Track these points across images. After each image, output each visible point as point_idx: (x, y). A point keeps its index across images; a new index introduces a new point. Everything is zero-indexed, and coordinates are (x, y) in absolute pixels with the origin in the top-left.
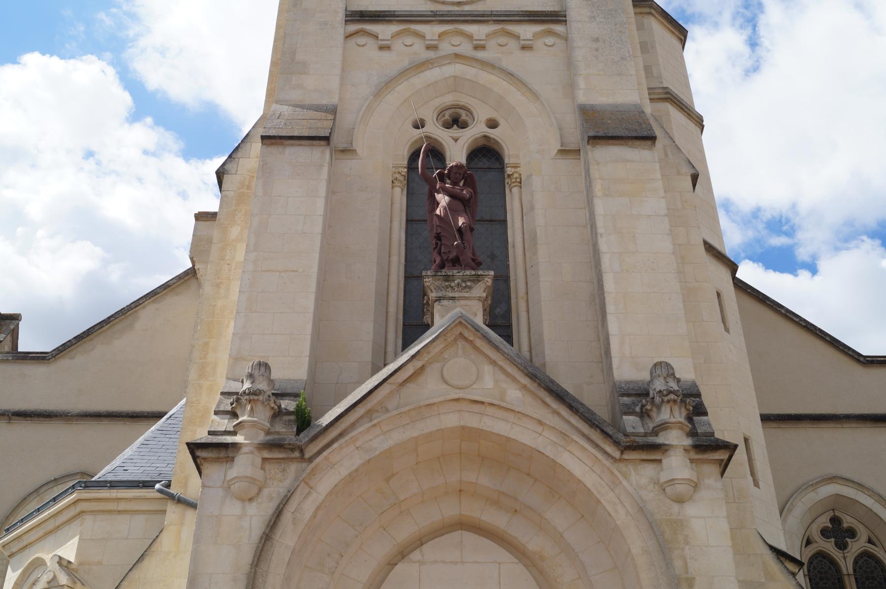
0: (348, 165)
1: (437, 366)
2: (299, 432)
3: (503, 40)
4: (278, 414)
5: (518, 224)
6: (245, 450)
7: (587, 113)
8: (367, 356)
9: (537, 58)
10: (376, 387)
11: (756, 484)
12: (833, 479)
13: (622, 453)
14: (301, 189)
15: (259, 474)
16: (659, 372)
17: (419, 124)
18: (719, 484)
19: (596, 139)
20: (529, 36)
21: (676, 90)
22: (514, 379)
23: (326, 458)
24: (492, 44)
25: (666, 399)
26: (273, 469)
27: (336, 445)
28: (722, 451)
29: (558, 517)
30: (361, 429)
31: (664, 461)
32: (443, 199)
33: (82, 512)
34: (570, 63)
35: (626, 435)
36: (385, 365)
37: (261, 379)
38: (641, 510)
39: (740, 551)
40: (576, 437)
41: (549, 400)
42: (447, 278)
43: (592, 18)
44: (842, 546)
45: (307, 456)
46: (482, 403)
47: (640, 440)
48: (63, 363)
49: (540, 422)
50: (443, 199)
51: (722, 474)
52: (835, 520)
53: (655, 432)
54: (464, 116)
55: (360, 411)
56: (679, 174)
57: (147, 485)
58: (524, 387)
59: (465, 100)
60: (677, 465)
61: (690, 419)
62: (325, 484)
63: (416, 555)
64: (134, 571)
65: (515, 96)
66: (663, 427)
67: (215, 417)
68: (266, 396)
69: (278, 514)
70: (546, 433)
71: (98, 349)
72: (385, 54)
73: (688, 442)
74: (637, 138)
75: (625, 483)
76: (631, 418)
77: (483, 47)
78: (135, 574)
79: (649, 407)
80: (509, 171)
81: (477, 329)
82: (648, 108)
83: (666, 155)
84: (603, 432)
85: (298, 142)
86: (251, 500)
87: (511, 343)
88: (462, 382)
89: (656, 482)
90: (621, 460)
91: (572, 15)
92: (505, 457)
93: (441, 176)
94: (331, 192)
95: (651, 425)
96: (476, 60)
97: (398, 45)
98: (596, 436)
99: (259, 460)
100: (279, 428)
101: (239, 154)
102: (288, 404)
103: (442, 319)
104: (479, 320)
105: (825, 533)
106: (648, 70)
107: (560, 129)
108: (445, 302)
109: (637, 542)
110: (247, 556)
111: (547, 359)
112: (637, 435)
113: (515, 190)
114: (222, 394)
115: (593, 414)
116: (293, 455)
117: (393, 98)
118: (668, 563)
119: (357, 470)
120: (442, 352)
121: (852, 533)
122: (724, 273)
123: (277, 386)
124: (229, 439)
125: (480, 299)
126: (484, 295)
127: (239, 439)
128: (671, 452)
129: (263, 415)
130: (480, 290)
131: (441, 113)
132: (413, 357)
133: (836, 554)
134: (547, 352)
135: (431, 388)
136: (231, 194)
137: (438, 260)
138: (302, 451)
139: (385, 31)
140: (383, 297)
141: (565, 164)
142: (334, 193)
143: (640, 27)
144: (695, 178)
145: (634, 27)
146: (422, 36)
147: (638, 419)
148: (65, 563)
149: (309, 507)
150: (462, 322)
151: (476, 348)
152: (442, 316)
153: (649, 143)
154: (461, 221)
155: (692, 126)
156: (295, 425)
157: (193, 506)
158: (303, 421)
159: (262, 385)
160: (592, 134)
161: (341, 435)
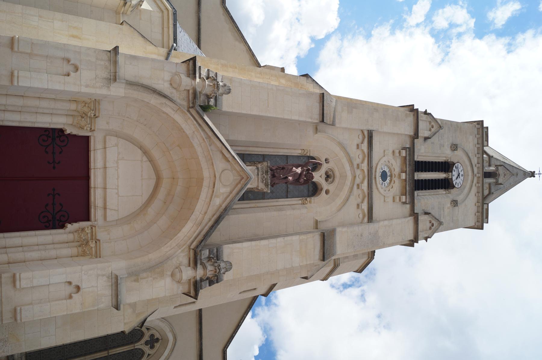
0: (311, 131)
1: (229, 167)
2: (201, 106)
3: (361, 196)
4: (208, 97)
5: (287, 203)
6: (193, 82)
7: (333, 232)
8: (231, 138)
9: (353, 211)
10: (220, 141)
11: (175, 307)
12: (175, 338)
13: (193, 249)
14: (303, 111)
15: (182, 88)
16: (228, 264)
17: (327, 161)
18: (180, 292)
19: (323, 236)
20: (363, 207)
21: (339, 269)
22: (224, 201)
23: (189, 118)
24: (360, 192)
25: (217, 268)
26: (184, 94)
27: (195, 122)
28: (194, 293)
29: (163, 222)
30: (202, 133)
31: (189, 268)
32: (299, 170)
33: (163, 12)
34: (352, 224)
35: (200, 251)
36: (230, 146)
37: (224, 90)
38: (168, 258)
39: (149, 302)
40: (200, 228)
41: (215, 217)
42: (267, 172)
43: (370, 234)
44: (147, 343)
45: (190, 110)
46: (214, 187)
47: (198, 257)
48: (221, 11)
49: (206, 213)
50: (299, 170)
51: (184, 294)
52: (157, 340)
53: (202, 264)
54: (330, 180)
55: (210, 133)
56: (308, 271)
57: (175, 40)
58: (221, 206)
59: (337, 180)
60: (188, 274)
61: (208, 279)
62: (178, 118)
63: (145, 159)
64: (137, 33)
65: (339, 201)
66: (205, 267)
67: (206, 69)
68: (216, 92)
69: (165, 96)
70: (201, 216)
71: (228, 26)
72: (355, 147)
73: (198, 278)
74: (324, 253)
75: (180, 251)
76: (208, 253)
77: (358, 188)
78: (136, 34)
79: (213, 260)
80: (308, 199)
81: (246, 185)
82: (333, 258)
83: (316, 266)
84: (202, 241)
85: (321, 108)
86: (171, 84)
87: (239, 200)
88: (222, 180)
89: (180, 265)
90: (190, 249)
91: (371, 225)
92: (190, 198)
93: (308, 170)
94: (300, 122)
95: (205, 262)
96: (353, 185)
97: (359, 152)
98: (200, 238)
99: (188, 88)
100: (202, 98)
101: (315, 84)
103: (249, 169)
104: (249, 186)
105: (152, 336)
106: (347, 257)
107: (326, 221)
108: (256, 171)
109: (154, 256)
110: (146, 82)
111: (231, 216)
112: (201, 256)
113: (300, 202)
114: (216, 73)
115: (209, 236)
116: (190, 103)
118: (145, 271)
119: (184, 132)
120: (235, 169)
121: (152, 347)
122: (264, 291)
123: (220, 97)
124: (197, 75)
125: (258, 186)
126: (260, 188)
127: (198, 80)
128: (194, 271)
129: (208, 90)
130: (262, 186)
131: (331, 170)
132: (234, 157)
133: (143, 341)
134: (234, 216)
135: (220, 165)
136: (298, 80)
137: (273, 168)
138: (192, 107)
140: (256, 145)
141: (312, 223)
142: (299, 124)
143: (363, 254)
144: (306, 278)
145: (364, 252)
146: (362, 162)
147: (207, 257)
148: (141, 3)
149: (168, 110)
150: (248, 178)
151: (237, 185)
152: (250, 170)
153: (322, 258)
154: (290, 178)
155: (324, 276)
156: (203, 105)
157: (167, 59)
158: (205, 108)
159: (221, 91)
160: (325, 234)
161: (199, 125)
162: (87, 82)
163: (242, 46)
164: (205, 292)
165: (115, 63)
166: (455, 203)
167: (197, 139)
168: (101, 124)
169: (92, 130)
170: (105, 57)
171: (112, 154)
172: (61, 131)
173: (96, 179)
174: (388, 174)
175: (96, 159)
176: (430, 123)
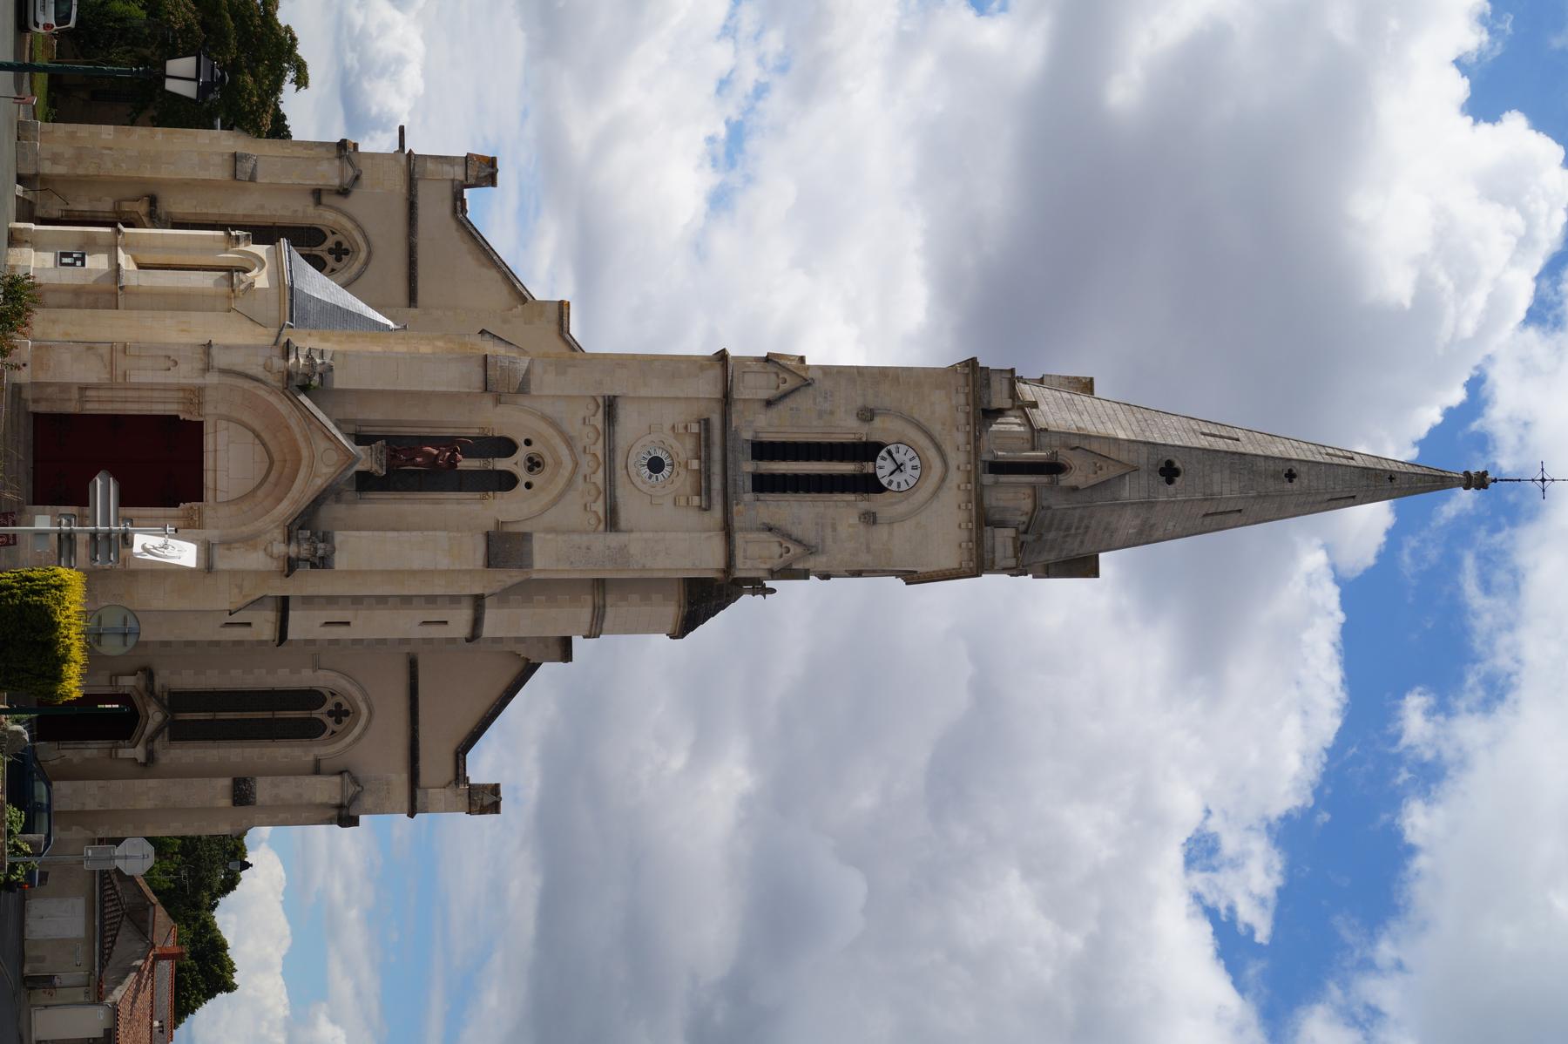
44: (330, 714)
48: (453, 225)
52: (347, 713)
60: (280, 548)
62: (272, 399)
71: (463, 247)
102: (316, 380)
105: (339, 705)
121: (339, 722)
127: (292, 360)
130: (375, 467)
133: (325, 709)
139: (598, 420)
162: (186, 374)
163: (493, 274)
164: (304, 571)
166: (870, 518)
167: (294, 421)
168: (209, 409)
170: (200, 350)
171: (222, 437)
172: (174, 419)
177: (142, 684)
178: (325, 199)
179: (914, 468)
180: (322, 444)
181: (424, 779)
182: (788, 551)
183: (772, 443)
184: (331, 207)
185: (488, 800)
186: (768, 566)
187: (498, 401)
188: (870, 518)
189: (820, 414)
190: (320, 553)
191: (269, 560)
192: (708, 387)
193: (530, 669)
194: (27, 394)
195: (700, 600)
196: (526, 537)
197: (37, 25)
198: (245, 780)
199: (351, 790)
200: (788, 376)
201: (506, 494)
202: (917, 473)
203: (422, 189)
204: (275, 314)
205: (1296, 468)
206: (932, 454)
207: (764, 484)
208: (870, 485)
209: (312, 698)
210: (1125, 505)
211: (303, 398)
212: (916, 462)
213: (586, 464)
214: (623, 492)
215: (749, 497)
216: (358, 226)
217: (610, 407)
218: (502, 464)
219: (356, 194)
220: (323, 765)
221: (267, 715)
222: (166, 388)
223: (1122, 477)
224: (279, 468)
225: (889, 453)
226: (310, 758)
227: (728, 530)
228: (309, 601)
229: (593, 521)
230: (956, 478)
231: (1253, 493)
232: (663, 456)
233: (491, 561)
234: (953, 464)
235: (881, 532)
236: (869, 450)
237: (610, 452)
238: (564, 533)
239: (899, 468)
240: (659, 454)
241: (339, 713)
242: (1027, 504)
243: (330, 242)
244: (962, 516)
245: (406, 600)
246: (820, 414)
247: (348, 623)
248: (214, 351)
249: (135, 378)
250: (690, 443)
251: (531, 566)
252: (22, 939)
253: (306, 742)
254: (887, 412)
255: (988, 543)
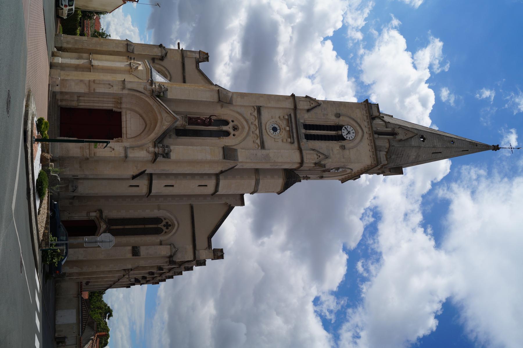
44: (164, 226)
48: (196, 71)
52: (170, 225)
62: (147, 99)
71: (201, 78)
102: (162, 94)
105: (167, 223)
117: (237, 116)
121: (167, 228)
127: (154, 86)
139: (255, 114)
149: (143, 97)
162: (116, 90)
165: (124, 84)
166: (343, 148)
167: (155, 107)
168: (124, 106)
169: (121, 108)
171: (128, 116)
172: (111, 111)
173: (124, 125)
174: (278, 128)
175: (124, 118)
176: (310, 102)
177: (98, 215)
178: (156, 61)
179: (353, 133)
180: (165, 115)
181: (198, 247)
182: (320, 157)
183: (309, 125)
184: (158, 64)
185: (219, 254)
186: (314, 162)
187: (222, 107)
188: (343, 148)
189: (324, 115)
190: (166, 151)
191: (148, 154)
192: (289, 105)
193: (230, 209)
194: (58, 97)
195: (291, 177)
196: (235, 150)
197: (62, 5)
198: (136, 247)
199: (174, 250)
200: (313, 104)
201: (227, 138)
202: (354, 134)
203: (187, 61)
204: (146, 78)
205: (454, 140)
206: (358, 128)
207: (309, 137)
208: (341, 138)
209: (158, 220)
210: (413, 147)
211: (158, 99)
212: (354, 131)
213: (253, 128)
214: (265, 137)
215: (305, 140)
216: (167, 69)
217: (259, 109)
218: (225, 128)
219: (166, 60)
220: (163, 242)
221: (142, 226)
222: (109, 94)
223: (411, 138)
224: (148, 126)
225: (345, 128)
226: (159, 240)
227: (300, 150)
228: (160, 176)
229: (257, 146)
230: (366, 136)
231: (445, 146)
232: (277, 126)
233: (225, 157)
234: (365, 132)
235: (347, 152)
236: (339, 128)
237: (260, 123)
238: (248, 149)
239: (349, 133)
240: (275, 126)
241: (167, 226)
242: (387, 145)
243: (164, 223)
244: (369, 148)
245: (193, 176)
246: (324, 115)
247: (173, 186)
248: (126, 83)
249: (98, 90)
250: (285, 122)
251: (237, 160)
252: (55, 324)
253: (157, 235)
254: (343, 115)
255: (379, 156)
